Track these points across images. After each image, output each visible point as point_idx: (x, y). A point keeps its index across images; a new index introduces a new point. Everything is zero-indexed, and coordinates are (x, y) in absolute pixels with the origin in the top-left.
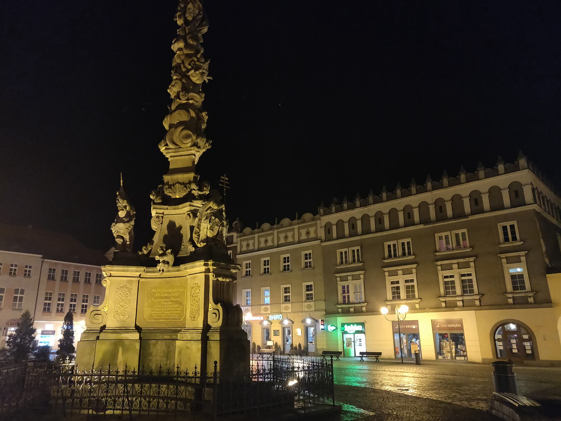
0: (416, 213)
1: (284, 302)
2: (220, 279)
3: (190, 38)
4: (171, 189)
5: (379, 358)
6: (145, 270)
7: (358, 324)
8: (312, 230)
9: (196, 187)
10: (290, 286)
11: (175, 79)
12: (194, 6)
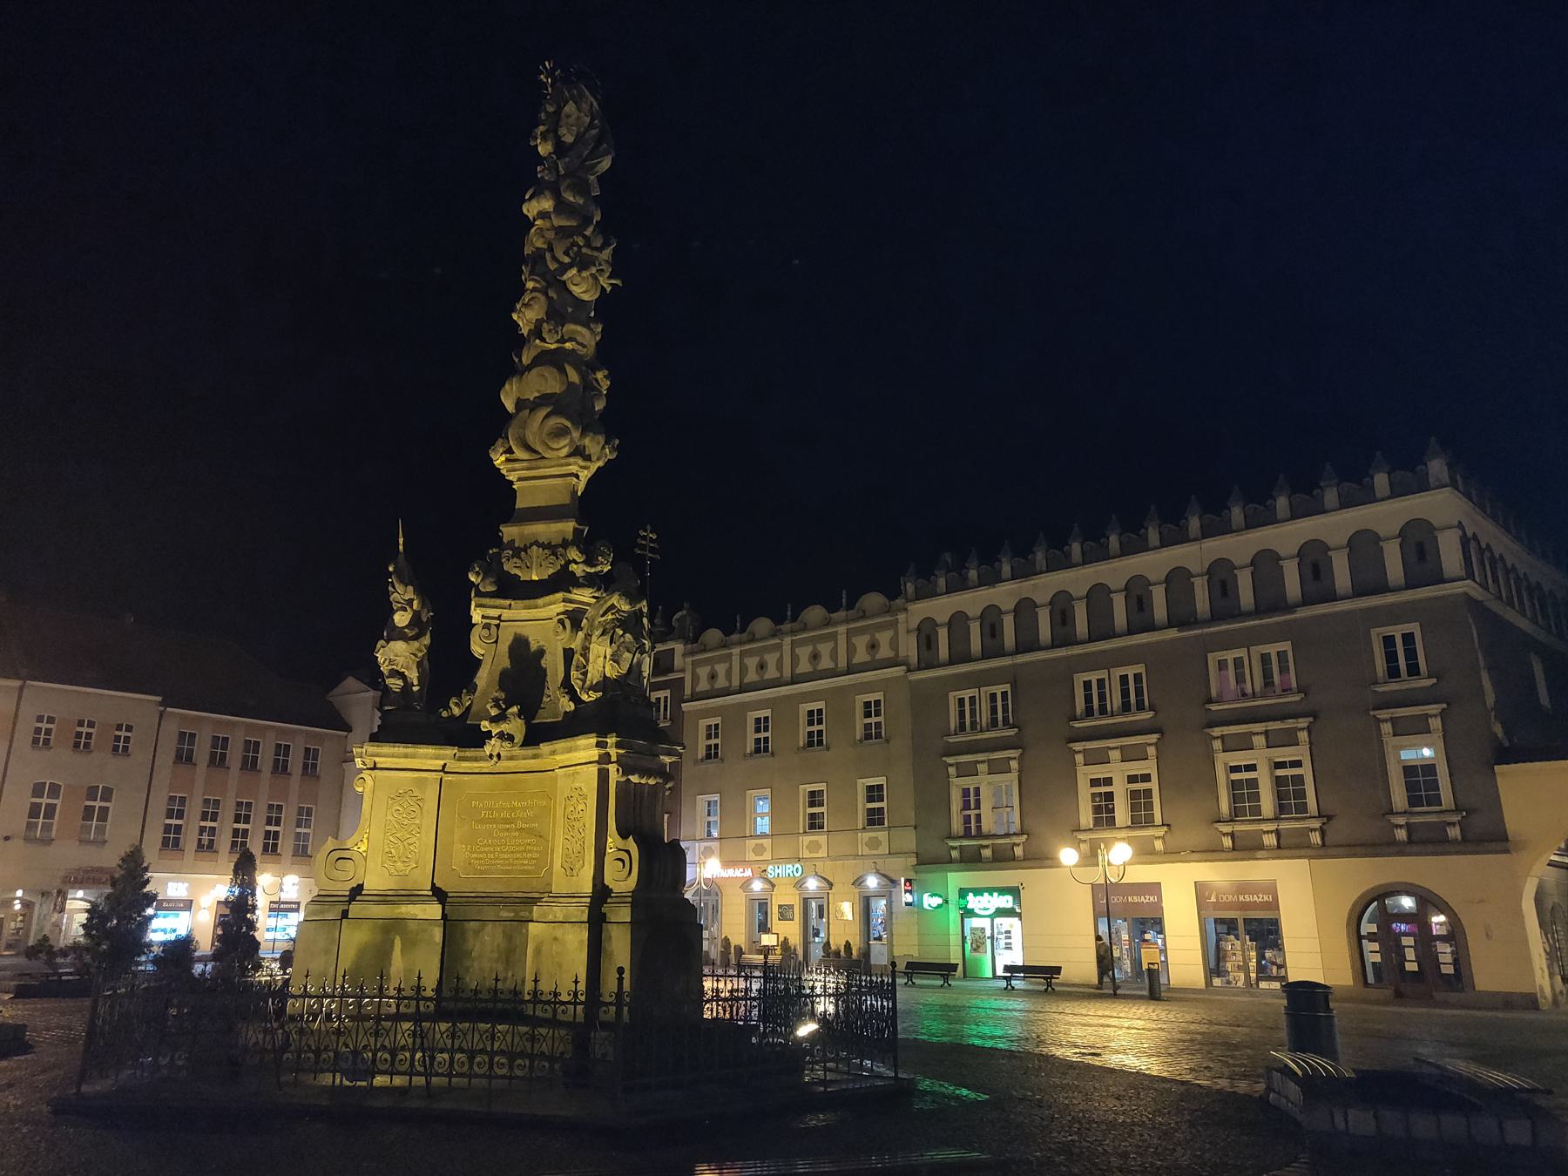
0: (1159, 597)
1: (807, 830)
2: (634, 779)
3: (568, 187)
4: (520, 558)
5: (1053, 980)
6: (455, 755)
7: (1003, 891)
8: (884, 638)
9: (580, 555)
10: (825, 789)
11: (531, 288)
12: (579, 109)
